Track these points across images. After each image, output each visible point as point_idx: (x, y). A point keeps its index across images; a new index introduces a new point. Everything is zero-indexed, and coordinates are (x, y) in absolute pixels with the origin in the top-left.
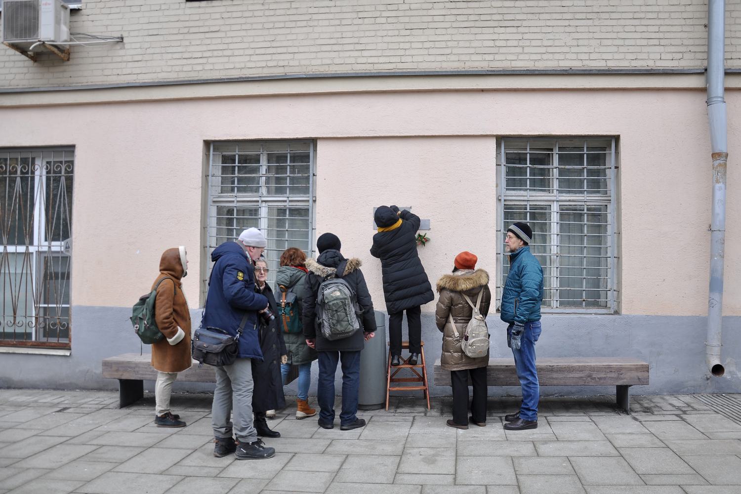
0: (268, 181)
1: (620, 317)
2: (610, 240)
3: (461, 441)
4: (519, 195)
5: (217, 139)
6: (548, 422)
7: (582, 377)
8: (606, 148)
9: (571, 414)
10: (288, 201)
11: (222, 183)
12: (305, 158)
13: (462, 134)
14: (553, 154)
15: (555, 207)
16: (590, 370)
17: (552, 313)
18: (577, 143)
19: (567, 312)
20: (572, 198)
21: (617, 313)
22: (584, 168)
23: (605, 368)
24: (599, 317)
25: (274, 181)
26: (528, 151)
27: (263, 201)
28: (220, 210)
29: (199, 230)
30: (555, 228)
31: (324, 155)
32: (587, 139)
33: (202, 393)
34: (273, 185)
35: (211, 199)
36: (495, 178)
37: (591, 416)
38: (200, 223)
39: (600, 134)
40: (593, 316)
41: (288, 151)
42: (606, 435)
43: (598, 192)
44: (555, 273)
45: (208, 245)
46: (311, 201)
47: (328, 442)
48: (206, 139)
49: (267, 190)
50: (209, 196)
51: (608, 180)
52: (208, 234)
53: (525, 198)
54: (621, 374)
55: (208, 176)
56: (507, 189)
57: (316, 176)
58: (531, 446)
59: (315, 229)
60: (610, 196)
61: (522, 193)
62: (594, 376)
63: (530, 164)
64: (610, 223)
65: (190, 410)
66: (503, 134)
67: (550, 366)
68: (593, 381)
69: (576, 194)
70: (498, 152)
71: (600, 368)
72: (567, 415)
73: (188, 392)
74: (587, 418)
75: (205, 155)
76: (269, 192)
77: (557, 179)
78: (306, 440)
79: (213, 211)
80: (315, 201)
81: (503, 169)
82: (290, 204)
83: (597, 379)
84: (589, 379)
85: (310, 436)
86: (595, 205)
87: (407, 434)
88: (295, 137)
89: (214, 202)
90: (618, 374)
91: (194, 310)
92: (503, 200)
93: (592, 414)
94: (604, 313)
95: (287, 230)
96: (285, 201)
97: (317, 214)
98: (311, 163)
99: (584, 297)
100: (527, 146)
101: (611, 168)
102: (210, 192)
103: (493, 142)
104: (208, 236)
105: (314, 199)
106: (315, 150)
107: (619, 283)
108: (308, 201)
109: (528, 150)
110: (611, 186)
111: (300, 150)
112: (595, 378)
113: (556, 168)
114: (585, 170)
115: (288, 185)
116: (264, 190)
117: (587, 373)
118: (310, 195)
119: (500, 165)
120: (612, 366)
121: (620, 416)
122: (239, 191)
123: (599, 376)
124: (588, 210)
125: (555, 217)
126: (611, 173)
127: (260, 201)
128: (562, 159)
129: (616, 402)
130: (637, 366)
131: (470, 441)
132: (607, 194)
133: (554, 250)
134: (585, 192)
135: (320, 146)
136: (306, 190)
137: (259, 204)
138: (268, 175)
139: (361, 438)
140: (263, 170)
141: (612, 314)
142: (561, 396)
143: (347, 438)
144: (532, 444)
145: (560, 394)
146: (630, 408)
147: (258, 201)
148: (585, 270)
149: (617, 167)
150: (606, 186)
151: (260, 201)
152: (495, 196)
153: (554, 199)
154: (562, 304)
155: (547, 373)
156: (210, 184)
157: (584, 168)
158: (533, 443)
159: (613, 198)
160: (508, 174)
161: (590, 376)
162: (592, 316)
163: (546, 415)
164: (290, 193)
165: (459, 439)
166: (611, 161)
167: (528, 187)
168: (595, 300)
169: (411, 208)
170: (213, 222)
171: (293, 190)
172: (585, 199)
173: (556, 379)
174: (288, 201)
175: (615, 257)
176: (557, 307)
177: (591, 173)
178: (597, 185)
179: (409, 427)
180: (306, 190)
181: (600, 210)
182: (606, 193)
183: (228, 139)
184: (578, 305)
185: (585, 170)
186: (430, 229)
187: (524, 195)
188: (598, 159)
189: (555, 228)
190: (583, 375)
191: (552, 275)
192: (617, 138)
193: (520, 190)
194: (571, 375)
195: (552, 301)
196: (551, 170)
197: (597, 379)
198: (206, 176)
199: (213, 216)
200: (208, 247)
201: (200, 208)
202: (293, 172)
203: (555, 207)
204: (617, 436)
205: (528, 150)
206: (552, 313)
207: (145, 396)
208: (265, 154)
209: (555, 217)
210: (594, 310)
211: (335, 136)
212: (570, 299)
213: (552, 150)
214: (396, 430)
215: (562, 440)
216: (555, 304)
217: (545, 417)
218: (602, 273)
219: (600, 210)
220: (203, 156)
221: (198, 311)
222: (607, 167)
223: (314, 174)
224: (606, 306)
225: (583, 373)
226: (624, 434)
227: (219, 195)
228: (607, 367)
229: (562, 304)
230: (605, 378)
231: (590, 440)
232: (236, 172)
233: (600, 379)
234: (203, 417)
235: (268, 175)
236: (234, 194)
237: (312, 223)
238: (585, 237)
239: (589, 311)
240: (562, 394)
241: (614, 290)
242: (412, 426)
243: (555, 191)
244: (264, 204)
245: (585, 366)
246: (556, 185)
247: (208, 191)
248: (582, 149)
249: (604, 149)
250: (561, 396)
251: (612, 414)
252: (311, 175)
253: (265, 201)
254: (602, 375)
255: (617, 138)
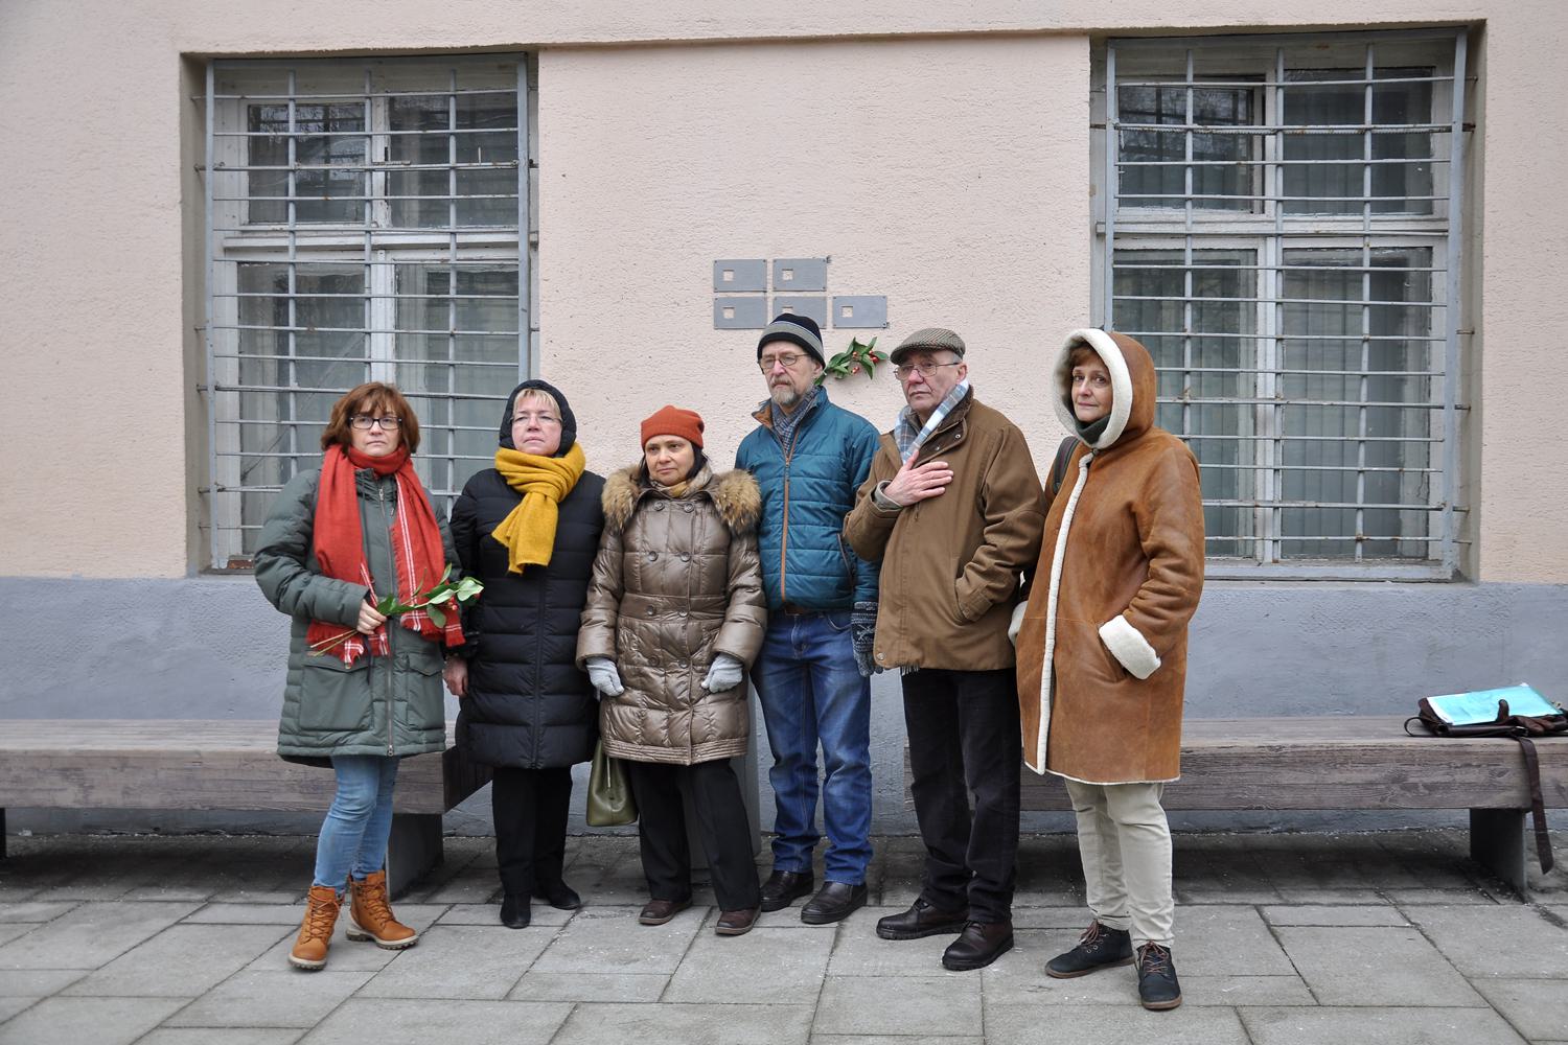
0: (394, 183)
1: (1474, 589)
2: (1442, 355)
3: (999, 1006)
4: (1159, 219)
5: (225, 48)
6: (1269, 926)
7: (1371, 783)
8: (1435, 67)
9: (1335, 898)
10: (453, 247)
11: (252, 192)
12: (506, 113)
13: (986, 28)
14: (1264, 87)
15: (1270, 255)
16: (1398, 761)
17: (1262, 580)
18: (1340, 55)
19: (1307, 576)
20: (1323, 228)
21: (1459, 577)
22: (1362, 133)
23: (1447, 753)
24: (1408, 589)
25: (415, 186)
26: (1190, 81)
27: (376, 248)
28: (249, 275)
29: (179, 337)
30: (1269, 320)
31: (561, 105)
32: (1376, 40)
33: (201, 832)
34: (413, 197)
35: (215, 243)
36: (1088, 164)
37: (1404, 904)
38: (179, 315)
39: (1422, 20)
40: (1389, 587)
41: (447, 94)
42: (1476, 983)
43: (1399, 207)
44: (1268, 455)
45: (210, 382)
46: (523, 247)
47: (559, 1014)
48: (188, 49)
49: (389, 212)
50: (209, 231)
51: (1436, 170)
52: (209, 349)
53: (1180, 229)
54: (1501, 774)
55: (204, 169)
56: (1123, 203)
57: (536, 166)
58: (1231, 1025)
59: (538, 330)
60: (1446, 220)
61: (1168, 213)
62: (1411, 780)
63: (1194, 122)
64: (1444, 302)
65: (141, 898)
66: (1113, 26)
67: (1270, 747)
68: (1408, 794)
69: (1335, 214)
70: (1095, 88)
71: (1430, 753)
72: (1325, 899)
73: (156, 830)
74: (1389, 914)
75: (189, 104)
76: (397, 216)
77: (1278, 165)
78: (489, 1008)
79: (225, 278)
80: (534, 245)
81: (1112, 140)
82: (463, 255)
83: (1421, 789)
84: (1396, 788)
85: (503, 989)
86: (1394, 248)
87: (821, 977)
88: (469, 43)
89: (228, 250)
90: (1492, 773)
91: (172, 580)
92: (1110, 236)
93: (1405, 897)
94: (1422, 576)
95: (452, 335)
96: (445, 247)
97: (542, 284)
98: (521, 128)
99: (1360, 530)
100: (1186, 69)
101: (1449, 130)
102: (209, 218)
103: (1079, 58)
104: (209, 355)
105: (533, 238)
106: (533, 87)
107: (1470, 484)
108: (514, 245)
109: (1190, 77)
110: (1447, 187)
111: (488, 88)
112: (1415, 786)
113: (1275, 132)
114: (1368, 138)
115: (453, 195)
116: (381, 214)
117: (1390, 768)
118: (522, 225)
119: (1104, 127)
120: (1469, 749)
121: (1495, 907)
122: (300, 217)
123: (1426, 780)
124: (1373, 262)
125: (1269, 286)
126: (1446, 149)
127: (368, 248)
128: (1296, 106)
129: (1468, 853)
130: (1551, 748)
131: (1026, 1005)
132: (1432, 213)
133: (1268, 386)
134: (1368, 208)
135: (549, 73)
136: (506, 213)
137: (366, 255)
138: (397, 165)
139: (668, 998)
140: (377, 150)
141: (1446, 582)
142: (1290, 830)
143: (625, 998)
144: (1235, 1017)
145: (1288, 826)
146: (1528, 883)
147: (360, 248)
148: (1362, 446)
149: (1469, 127)
150: (1429, 187)
151: (368, 248)
152: (1087, 220)
153: (1270, 230)
154: (1290, 551)
155: (1260, 769)
156: (209, 194)
157: (1362, 133)
158: (1238, 1014)
159: (1454, 226)
160: (1126, 151)
161: (1398, 779)
162: (1385, 587)
163: (1256, 899)
164: (459, 221)
165: (992, 1000)
166: (1449, 109)
167: (1189, 194)
168: (1388, 541)
169: (828, 260)
170: (226, 310)
171: (471, 213)
172: (1368, 230)
173: (1290, 787)
174: (453, 247)
175: (1456, 408)
176: (1275, 562)
177: (1384, 145)
178: (1399, 184)
179: (828, 950)
180: (506, 213)
181: (1402, 262)
182: (1428, 208)
183: (261, 50)
184: (1341, 552)
185: (1368, 138)
186: (886, 326)
187: (1174, 219)
188: (1406, 102)
189: (1269, 320)
190: (1377, 775)
191: (1260, 463)
192: (1473, 33)
193: (1161, 203)
194: (1337, 777)
195: (1259, 544)
196: (1257, 142)
197: (1421, 789)
198: (196, 171)
199: (228, 292)
200: (211, 389)
201: (178, 267)
202: (466, 153)
203: (1270, 255)
204: (1514, 986)
205: (1190, 77)
206: (1262, 580)
207: (9, 851)
208: (381, 102)
209: (1269, 286)
210: (1387, 568)
211: (592, 39)
212: (1313, 536)
213: (1262, 77)
214: (786, 960)
215: (1330, 1002)
216: (1268, 551)
217: (1258, 908)
218: (1407, 459)
219: (1402, 262)
220: (181, 104)
221: (182, 583)
222: (1435, 123)
223: (531, 162)
224: (1425, 557)
225: (1375, 771)
226: (1535, 978)
227: (243, 228)
228: (1456, 749)
229: (1290, 551)
230: (1447, 786)
231: (1426, 1002)
232: (292, 156)
233: (1432, 788)
234: (177, 923)
235: (397, 165)
236: (284, 227)
237: (528, 311)
238: (1366, 346)
239: (1378, 571)
240: (1295, 825)
241: (1455, 509)
242: (835, 947)
243: (1270, 206)
244: (381, 256)
245: (1382, 749)
246: (1274, 185)
247: (205, 217)
248: (1359, 71)
249: (1427, 70)
250: (1290, 830)
251: (1469, 898)
252: (522, 162)
253: (387, 248)
254: (1439, 777)
255: (1473, 33)
